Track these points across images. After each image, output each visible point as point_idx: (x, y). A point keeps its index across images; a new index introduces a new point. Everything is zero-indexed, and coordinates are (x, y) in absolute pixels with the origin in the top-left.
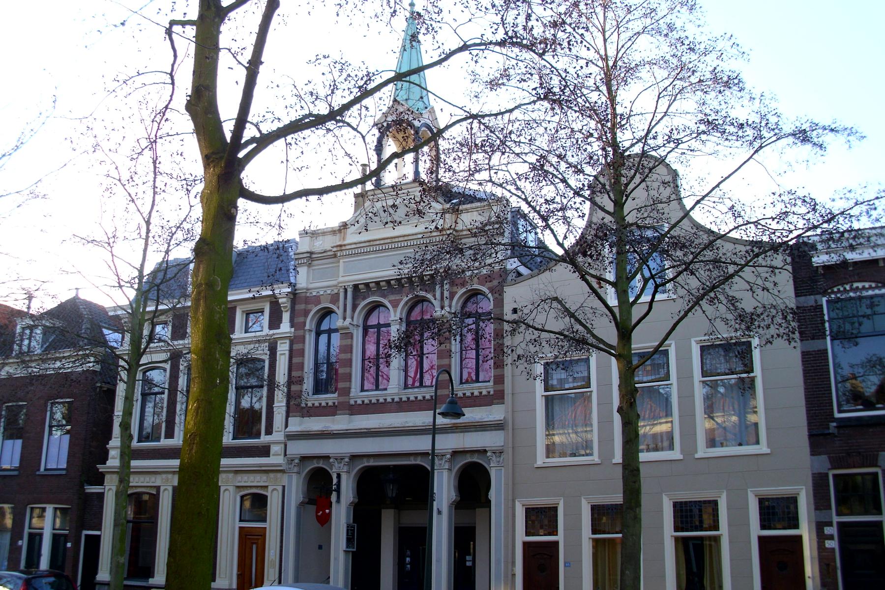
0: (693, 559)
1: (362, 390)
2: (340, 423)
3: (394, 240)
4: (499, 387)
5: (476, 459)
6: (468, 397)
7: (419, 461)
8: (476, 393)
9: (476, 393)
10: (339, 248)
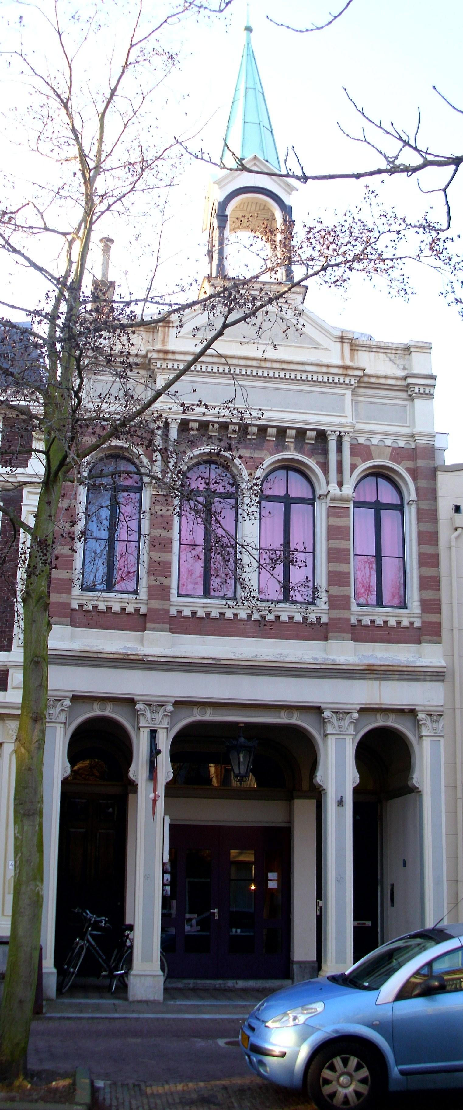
0: (379, 855)
1: (136, 592)
2: (157, 643)
3: (263, 364)
4: (432, 618)
5: (391, 722)
6: (379, 627)
7: (295, 720)
8: (392, 622)
9: (392, 622)
10: (161, 355)
